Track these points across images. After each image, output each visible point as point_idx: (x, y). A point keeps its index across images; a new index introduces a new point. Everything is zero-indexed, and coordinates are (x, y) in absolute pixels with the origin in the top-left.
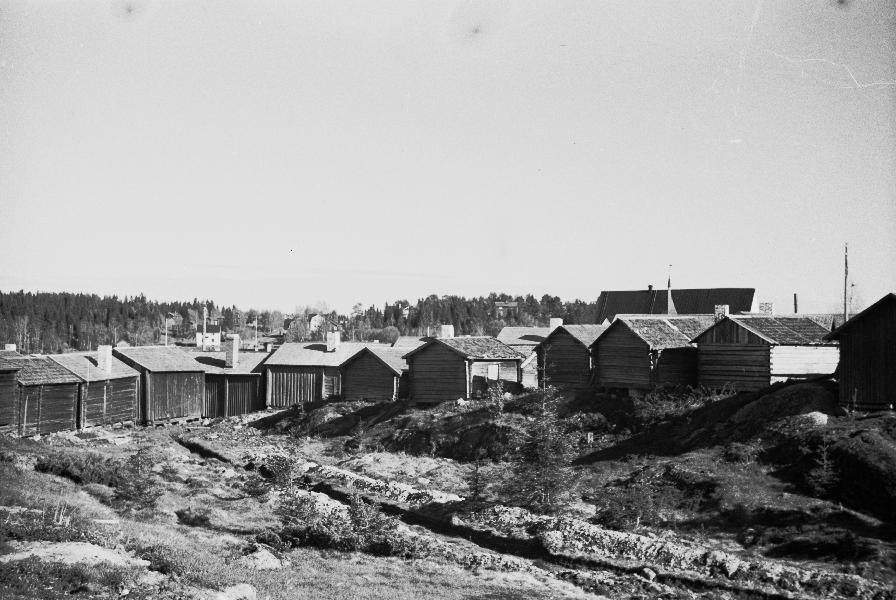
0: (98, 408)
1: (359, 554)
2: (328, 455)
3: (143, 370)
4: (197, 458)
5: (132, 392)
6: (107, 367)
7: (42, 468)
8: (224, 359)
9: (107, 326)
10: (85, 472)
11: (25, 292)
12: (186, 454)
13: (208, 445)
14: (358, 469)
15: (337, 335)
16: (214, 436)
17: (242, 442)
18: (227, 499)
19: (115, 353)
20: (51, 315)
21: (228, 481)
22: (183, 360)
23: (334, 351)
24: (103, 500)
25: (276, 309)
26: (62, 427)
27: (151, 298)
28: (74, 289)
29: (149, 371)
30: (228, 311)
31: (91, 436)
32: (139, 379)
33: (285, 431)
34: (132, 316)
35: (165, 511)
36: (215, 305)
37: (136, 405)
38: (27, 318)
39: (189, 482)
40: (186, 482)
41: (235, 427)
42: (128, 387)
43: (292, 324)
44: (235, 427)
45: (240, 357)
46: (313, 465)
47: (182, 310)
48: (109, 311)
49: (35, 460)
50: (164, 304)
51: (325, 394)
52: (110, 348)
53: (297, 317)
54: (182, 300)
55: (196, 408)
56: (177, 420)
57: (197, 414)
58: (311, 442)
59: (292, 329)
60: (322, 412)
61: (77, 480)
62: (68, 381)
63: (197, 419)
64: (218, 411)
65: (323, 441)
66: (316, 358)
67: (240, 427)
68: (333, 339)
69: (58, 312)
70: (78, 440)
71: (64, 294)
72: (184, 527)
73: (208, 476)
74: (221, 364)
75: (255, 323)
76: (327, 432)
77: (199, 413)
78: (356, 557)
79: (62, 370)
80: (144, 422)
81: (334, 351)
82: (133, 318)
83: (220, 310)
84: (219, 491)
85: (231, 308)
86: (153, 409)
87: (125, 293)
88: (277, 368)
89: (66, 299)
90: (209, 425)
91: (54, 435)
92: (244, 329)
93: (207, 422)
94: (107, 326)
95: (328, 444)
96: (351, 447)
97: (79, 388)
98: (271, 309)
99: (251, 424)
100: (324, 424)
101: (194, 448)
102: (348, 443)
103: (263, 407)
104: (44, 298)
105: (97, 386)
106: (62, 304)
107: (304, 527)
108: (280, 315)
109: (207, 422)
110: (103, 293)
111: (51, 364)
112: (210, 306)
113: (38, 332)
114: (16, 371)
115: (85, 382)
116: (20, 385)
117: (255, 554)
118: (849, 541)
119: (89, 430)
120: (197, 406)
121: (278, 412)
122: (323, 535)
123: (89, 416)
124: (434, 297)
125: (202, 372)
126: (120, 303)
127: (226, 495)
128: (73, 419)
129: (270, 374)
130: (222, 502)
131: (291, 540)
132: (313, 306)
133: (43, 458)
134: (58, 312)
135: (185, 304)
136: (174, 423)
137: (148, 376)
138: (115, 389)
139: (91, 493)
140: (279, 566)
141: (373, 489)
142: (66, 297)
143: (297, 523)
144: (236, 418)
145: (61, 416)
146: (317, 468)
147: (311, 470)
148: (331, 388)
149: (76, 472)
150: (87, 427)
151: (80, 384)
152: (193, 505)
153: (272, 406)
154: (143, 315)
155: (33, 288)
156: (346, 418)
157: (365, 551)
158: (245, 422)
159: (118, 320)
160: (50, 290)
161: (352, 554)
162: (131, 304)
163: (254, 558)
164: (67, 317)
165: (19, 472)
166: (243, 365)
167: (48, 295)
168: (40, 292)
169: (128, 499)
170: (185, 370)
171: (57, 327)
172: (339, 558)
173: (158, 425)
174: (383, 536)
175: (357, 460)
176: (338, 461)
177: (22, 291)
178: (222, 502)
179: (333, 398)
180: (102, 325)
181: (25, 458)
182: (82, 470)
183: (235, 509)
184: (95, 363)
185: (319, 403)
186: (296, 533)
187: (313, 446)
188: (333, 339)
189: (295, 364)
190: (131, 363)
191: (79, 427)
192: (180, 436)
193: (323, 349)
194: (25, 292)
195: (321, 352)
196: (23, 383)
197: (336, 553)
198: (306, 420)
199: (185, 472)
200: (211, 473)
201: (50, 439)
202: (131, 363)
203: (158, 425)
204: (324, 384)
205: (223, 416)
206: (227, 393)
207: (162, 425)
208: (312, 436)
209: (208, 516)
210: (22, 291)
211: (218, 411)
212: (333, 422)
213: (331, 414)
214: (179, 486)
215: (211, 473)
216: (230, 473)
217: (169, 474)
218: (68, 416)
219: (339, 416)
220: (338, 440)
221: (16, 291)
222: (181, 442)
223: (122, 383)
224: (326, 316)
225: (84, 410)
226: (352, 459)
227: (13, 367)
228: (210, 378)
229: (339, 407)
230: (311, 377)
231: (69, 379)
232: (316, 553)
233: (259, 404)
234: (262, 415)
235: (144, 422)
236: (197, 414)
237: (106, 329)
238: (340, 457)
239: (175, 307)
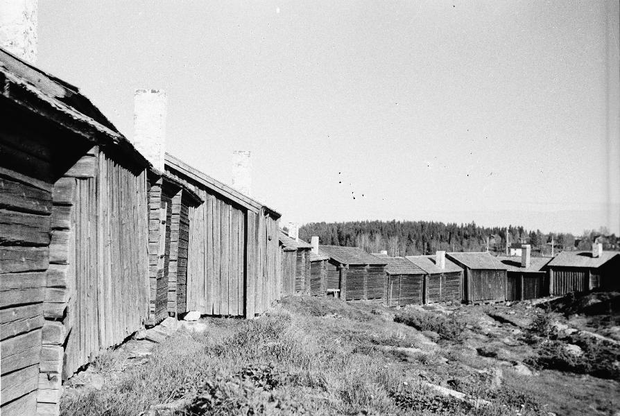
0: (437, 291)
1: (588, 375)
2: (589, 327)
3: (465, 267)
4: (498, 323)
5: (458, 282)
6: (442, 264)
7: (397, 320)
8: (520, 262)
9: (449, 243)
10: (423, 324)
11: (397, 221)
12: (491, 321)
13: (507, 317)
14: (608, 335)
15: (600, 246)
16: (512, 312)
17: (525, 313)
18: (511, 346)
19: (447, 256)
20: (412, 236)
21: (515, 336)
22: (495, 262)
23: (597, 257)
24: (432, 339)
25: (569, 232)
26: (414, 302)
27: (479, 225)
28: (428, 219)
29: (469, 269)
30: (534, 234)
31: (431, 308)
32: (463, 273)
33: (560, 311)
34: (466, 237)
35: (469, 347)
36: (524, 229)
37: (461, 290)
38: (397, 237)
39: (489, 335)
40: (487, 335)
41: (527, 307)
42: (456, 278)
43: (580, 243)
44: (527, 307)
45: (531, 261)
46: (575, 330)
47: (501, 233)
48: (450, 234)
49: (393, 315)
50: (488, 229)
51: (591, 287)
52: (444, 253)
53: (585, 238)
54: (501, 226)
55: (501, 292)
56: (488, 301)
57: (502, 298)
58: (578, 318)
59: (560, 242)
60: (587, 298)
61: (419, 328)
62: (417, 273)
63: (502, 302)
64: (516, 296)
65: (586, 317)
66: (585, 262)
67: (530, 307)
68: (598, 249)
69: (417, 234)
70: (423, 310)
71: (421, 222)
72: (481, 357)
73: (503, 333)
74: (518, 265)
75: (553, 243)
76: (589, 311)
77: (504, 298)
78: (585, 378)
79: (414, 267)
80: (465, 302)
81: (597, 257)
82: (467, 238)
83: (528, 233)
84: (507, 340)
85: (536, 232)
86: (473, 293)
87: (461, 221)
88: (556, 269)
89: (422, 226)
90: (510, 306)
91: (408, 306)
92: (544, 247)
93: (509, 304)
94: (449, 243)
95: (590, 319)
96: (605, 323)
97: (424, 278)
98: (565, 232)
99: (538, 306)
100: (588, 307)
101: (497, 318)
102: (605, 319)
103: (547, 294)
104: (409, 225)
105: (435, 277)
106: (420, 229)
107: (551, 357)
108: (573, 237)
109: (509, 304)
110: (447, 221)
111: (407, 262)
112: (521, 230)
113: (404, 247)
114: (385, 265)
115: (428, 274)
116: (388, 274)
117: (516, 366)
118: (343, 239)
119: (431, 305)
120: (502, 293)
121: (557, 298)
122: (564, 362)
123: (431, 296)
124: (455, 225)
125: (505, 270)
126: (458, 228)
127: (512, 344)
128: (421, 297)
129: (552, 272)
130: (507, 346)
131: (543, 364)
132: (597, 230)
133: (398, 314)
134: (417, 234)
135: (503, 228)
136: (486, 304)
137: (468, 271)
138: (447, 279)
139: (426, 336)
140: (531, 375)
141: (614, 346)
142: (423, 225)
143: (548, 355)
144: (529, 302)
145: (414, 295)
146: (577, 332)
147: (573, 333)
148: (595, 283)
149: (418, 323)
150: (429, 303)
151: (425, 275)
152: (488, 347)
153: (554, 294)
154: (473, 236)
155: (400, 218)
156: (604, 302)
157: (592, 374)
158: (534, 304)
159: (457, 239)
160: (411, 220)
161: (583, 375)
162: (466, 229)
163: (515, 368)
164: (423, 237)
165: (384, 321)
166: (533, 265)
167: (411, 223)
168: (406, 221)
169: (448, 339)
170: (487, 268)
171: (416, 244)
172: (573, 377)
173: (475, 304)
174: (604, 366)
175: (607, 329)
176: (595, 330)
177: (394, 220)
178: (507, 346)
179: (594, 290)
180: (446, 243)
181: (388, 314)
182: (421, 322)
183: (517, 351)
184: (435, 262)
185: (587, 291)
186: (546, 360)
187: (578, 320)
188: (598, 249)
189: (561, 265)
190: (457, 263)
191: (424, 303)
192: (490, 312)
193: (590, 255)
194: (397, 221)
195: (588, 258)
196: (390, 273)
197: (572, 374)
198: (576, 303)
199: (488, 330)
200: (505, 331)
201: (406, 309)
202: (457, 263)
203: (475, 304)
204: (590, 280)
205: (520, 300)
206: (523, 285)
207: (479, 304)
208: (579, 315)
209: (496, 352)
210: (394, 220)
211: (516, 296)
212: (594, 305)
213: (593, 300)
214: (482, 337)
215: (505, 331)
216: (517, 331)
217: (476, 329)
218: (418, 295)
219: (599, 301)
220: (597, 317)
221: (374, 220)
222: (490, 315)
223: (453, 275)
224: (608, 237)
225: (427, 292)
226: (604, 328)
227: (384, 263)
228: (510, 274)
229: (598, 295)
230: (580, 275)
231: (417, 272)
232: (559, 374)
233: (544, 292)
234: (545, 300)
235: (465, 302)
236: (502, 298)
237: (448, 246)
238: (597, 327)
239: (496, 231)
